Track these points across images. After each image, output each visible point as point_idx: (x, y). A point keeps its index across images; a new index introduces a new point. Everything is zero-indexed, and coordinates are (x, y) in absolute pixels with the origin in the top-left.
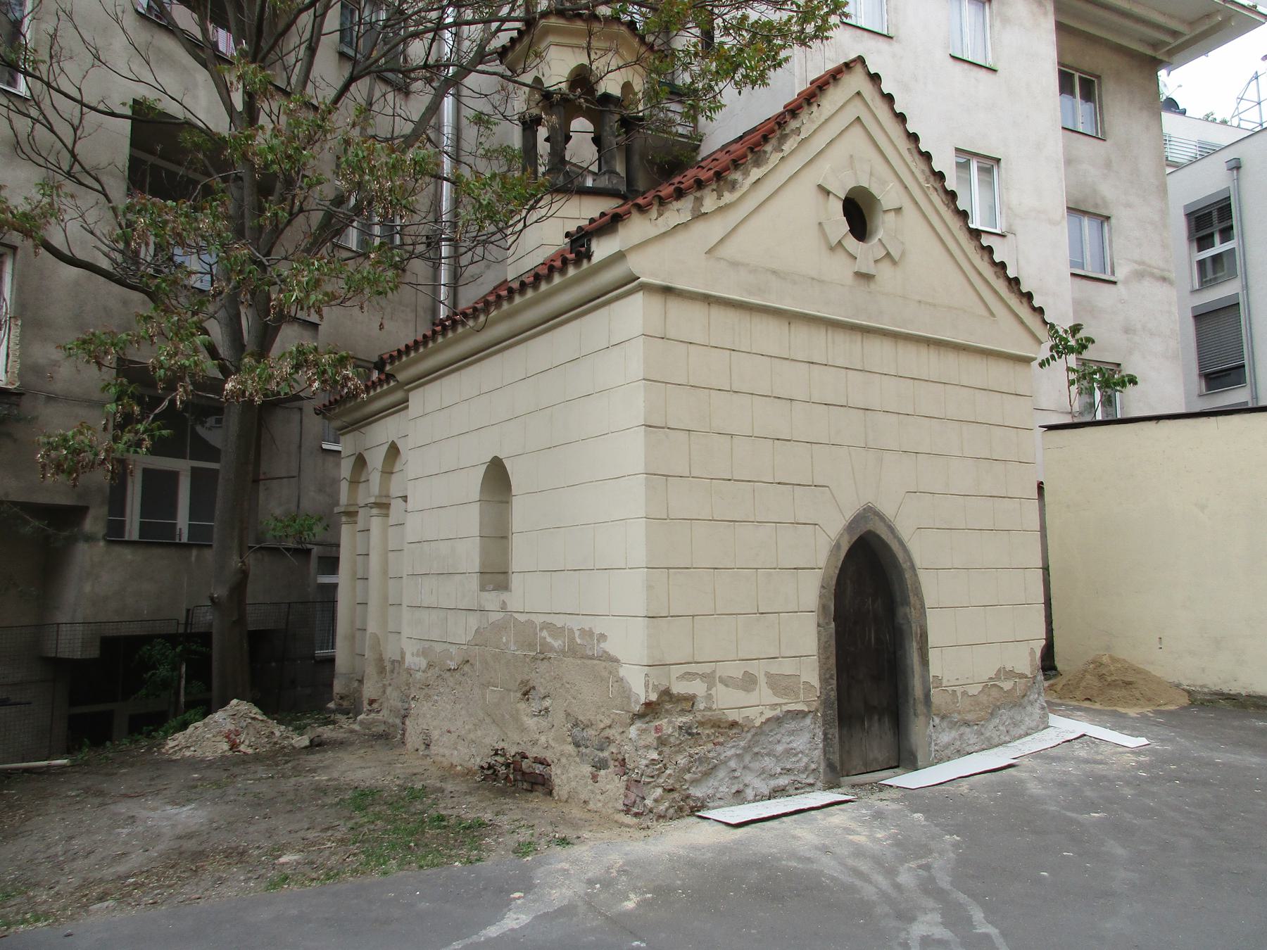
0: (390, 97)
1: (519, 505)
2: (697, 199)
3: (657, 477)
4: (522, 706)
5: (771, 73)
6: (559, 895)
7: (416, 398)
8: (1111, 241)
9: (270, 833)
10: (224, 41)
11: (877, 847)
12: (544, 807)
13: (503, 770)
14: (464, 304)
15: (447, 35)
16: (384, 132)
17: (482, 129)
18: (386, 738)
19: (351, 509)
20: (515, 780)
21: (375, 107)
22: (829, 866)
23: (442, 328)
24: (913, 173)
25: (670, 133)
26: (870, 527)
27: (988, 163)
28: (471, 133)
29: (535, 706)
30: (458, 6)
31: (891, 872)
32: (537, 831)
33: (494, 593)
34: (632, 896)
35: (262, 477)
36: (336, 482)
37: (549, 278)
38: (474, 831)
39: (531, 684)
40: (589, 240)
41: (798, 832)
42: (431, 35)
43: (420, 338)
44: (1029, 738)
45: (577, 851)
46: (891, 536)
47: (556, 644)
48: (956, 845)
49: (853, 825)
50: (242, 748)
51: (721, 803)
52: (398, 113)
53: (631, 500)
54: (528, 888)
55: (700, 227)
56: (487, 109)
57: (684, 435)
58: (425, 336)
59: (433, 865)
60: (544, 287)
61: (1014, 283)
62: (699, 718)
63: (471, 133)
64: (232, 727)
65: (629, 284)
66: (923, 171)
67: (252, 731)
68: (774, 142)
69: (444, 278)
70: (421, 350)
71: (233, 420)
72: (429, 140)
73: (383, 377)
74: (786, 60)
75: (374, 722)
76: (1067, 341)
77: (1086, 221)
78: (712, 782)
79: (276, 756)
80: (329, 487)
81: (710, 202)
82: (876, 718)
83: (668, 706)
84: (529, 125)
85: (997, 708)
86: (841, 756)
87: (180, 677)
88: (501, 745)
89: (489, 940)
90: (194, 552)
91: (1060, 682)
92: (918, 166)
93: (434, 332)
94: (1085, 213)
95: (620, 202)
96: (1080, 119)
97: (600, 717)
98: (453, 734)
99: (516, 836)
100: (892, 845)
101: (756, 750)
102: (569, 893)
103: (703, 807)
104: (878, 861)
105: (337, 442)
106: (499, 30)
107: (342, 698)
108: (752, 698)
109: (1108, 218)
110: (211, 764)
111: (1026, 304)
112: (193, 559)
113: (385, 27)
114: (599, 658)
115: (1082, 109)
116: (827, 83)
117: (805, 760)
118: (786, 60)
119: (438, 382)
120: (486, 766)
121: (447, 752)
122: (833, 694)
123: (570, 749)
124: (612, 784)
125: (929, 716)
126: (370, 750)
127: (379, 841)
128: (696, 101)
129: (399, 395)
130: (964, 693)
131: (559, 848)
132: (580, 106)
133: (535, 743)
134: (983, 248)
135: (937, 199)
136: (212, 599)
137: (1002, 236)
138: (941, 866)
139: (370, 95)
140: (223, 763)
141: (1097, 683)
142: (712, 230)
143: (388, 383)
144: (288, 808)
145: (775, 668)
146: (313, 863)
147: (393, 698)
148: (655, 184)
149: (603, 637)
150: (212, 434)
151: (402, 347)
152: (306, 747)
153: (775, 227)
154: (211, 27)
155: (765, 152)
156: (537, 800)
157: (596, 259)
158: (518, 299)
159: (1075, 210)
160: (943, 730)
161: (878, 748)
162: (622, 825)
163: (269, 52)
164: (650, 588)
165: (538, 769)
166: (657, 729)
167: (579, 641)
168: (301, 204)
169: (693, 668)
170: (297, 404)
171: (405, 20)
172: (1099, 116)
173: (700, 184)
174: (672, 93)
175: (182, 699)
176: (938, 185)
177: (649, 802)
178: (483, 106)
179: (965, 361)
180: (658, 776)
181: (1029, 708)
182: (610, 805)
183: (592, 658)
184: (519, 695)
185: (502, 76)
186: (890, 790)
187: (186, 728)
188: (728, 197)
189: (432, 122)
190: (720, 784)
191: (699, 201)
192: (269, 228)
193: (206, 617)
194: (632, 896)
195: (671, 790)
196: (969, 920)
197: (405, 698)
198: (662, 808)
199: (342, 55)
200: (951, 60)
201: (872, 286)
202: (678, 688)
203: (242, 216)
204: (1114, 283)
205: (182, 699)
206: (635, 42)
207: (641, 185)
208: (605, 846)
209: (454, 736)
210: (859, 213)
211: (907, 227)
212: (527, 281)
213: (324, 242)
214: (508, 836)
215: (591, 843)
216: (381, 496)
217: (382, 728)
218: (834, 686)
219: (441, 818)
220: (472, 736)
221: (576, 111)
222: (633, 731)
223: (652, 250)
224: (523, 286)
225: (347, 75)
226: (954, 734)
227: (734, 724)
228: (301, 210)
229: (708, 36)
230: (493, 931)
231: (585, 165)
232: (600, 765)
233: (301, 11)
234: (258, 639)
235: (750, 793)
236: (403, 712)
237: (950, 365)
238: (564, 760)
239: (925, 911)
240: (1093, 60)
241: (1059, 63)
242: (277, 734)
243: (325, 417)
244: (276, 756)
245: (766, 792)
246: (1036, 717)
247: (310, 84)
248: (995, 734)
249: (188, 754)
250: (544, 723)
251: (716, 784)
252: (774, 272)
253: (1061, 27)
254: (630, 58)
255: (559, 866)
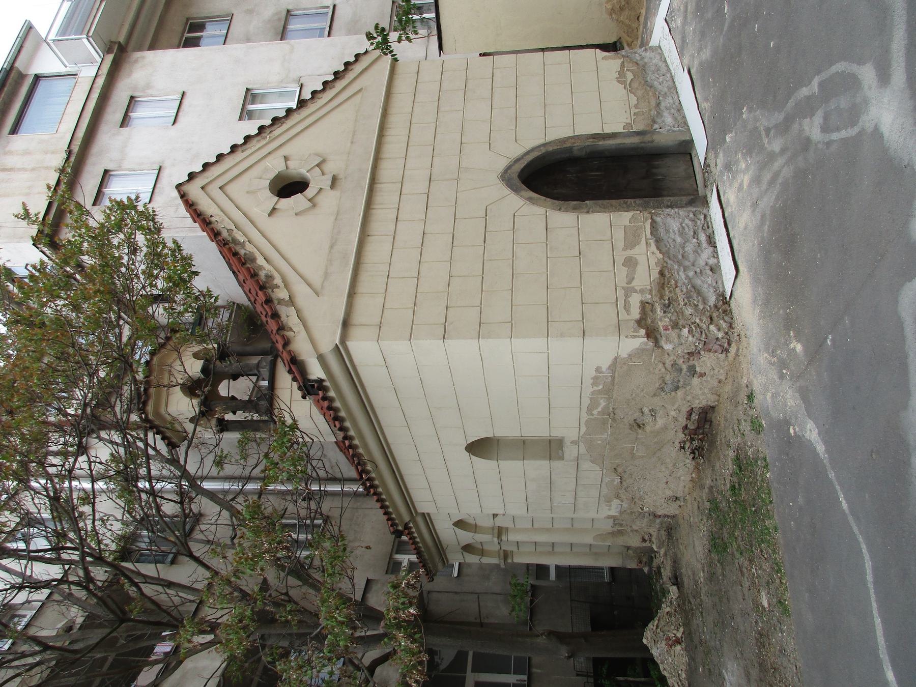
0: (203, 527)
1: (501, 431)
2: (279, 303)
3: (481, 330)
4: (648, 429)
5: (184, 253)
6: (792, 400)
7: (422, 508)
8: (305, 9)
9: (745, 614)
10: (162, 648)
11: (753, 167)
12: (723, 412)
13: (696, 443)
14: (353, 474)
15: (158, 486)
16: (229, 532)
17: (226, 461)
18: (670, 529)
19: (502, 554)
20: (703, 434)
21: (211, 538)
22: (767, 202)
23: (371, 489)
24: (259, 149)
25: (228, 326)
26: (515, 176)
27: (249, 96)
28: (229, 469)
29: (648, 419)
30: (137, 479)
31: (772, 157)
32: (742, 417)
33: (565, 449)
34: (792, 346)
35: (478, 621)
36: (481, 566)
37: (336, 410)
38: (742, 463)
39: (632, 422)
40: (309, 380)
41: (742, 225)
42: (158, 500)
43: (378, 505)
44: (668, 59)
45: (757, 387)
46: (522, 161)
47: (603, 403)
48: (750, 110)
49: (736, 185)
50: (679, 635)
51: (720, 282)
52: (215, 521)
53: (498, 348)
54: (787, 423)
55: (300, 301)
56: (211, 457)
57: (450, 310)
58: (378, 501)
59: (769, 493)
60: (342, 414)
61: (338, 75)
62: (657, 299)
63: (229, 469)
64: (664, 643)
65: (341, 351)
66: (258, 141)
67: (666, 628)
68: (238, 248)
69: (337, 488)
70: (387, 503)
71: (436, 642)
72: (233, 499)
73: (407, 531)
74: (175, 242)
75: (658, 538)
76: (378, 43)
77: (290, 27)
78: (705, 289)
79: (685, 610)
80: (485, 572)
81: (281, 294)
82: (654, 171)
83: (649, 321)
84: (223, 426)
85: (647, 82)
86: (684, 195)
87: (626, 681)
88: (677, 445)
89: (827, 451)
90: (534, 670)
91: (626, 39)
92: (254, 145)
93: (375, 494)
94: (284, 28)
95: (279, 360)
96: (218, 32)
97: (657, 371)
98: (668, 480)
99: (746, 433)
100: (751, 157)
101: (680, 257)
102: (790, 392)
103: (723, 295)
104: (763, 167)
105: (452, 566)
106: (155, 449)
107: (640, 562)
108: (642, 260)
109: (288, 11)
110: (692, 659)
111: (353, 67)
112: (539, 671)
113: (153, 532)
114: (614, 372)
115: (211, 30)
116: (195, 210)
117: (687, 221)
118: (175, 242)
119: (410, 491)
120: (692, 456)
121: (682, 484)
122: (638, 201)
123: (680, 393)
124: (706, 362)
125: (653, 132)
126: (680, 541)
127: (750, 533)
128: (204, 307)
129: (420, 520)
130: (636, 107)
131: (756, 401)
132: (209, 391)
133: (676, 419)
134: (312, 98)
135: (278, 131)
136: (569, 657)
137: (301, 86)
138: (766, 120)
139: (202, 541)
140: (691, 650)
141: (627, 12)
142: (301, 291)
143: (411, 528)
144: (725, 600)
145: (620, 244)
146: (768, 582)
147: (641, 524)
148: (267, 335)
149: (598, 370)
150: (447, 656)
151: (385, 517)
152: (678, 588)
153: (299, 247)
154: (153, 658)
155: (245, 254)
156: (719, 418)
157: (322, 376)
158: (352, 433)
159: (283, 35)
160: (663, 121)
161: (677, 169)
162: (737, 355)
163: (172, 616)
164: (562, 335)
165: (695, 417)
166: (666, 329)
167: (601, 387)
168: (282, 594)
169: (621, 303)
170: (425, 595)
171: (148, 516)
172: (215, 19)
173: (269, 301)
174: (200, 324)
175: (643, 679)
176: (268, 131)
177: (720, 335)
178: (209, 460)
179: (395, 109)
180: (700, 328)
181: (646, 60)
182: (722, 363)
183: (613, 378)
184: (640, 431)
185: (189, 447)
186: (709, 158)
187: (664, 677)
188: (278, 281)
189: (222, 497)
190: (706, 283)
191: (280, 301)
192: (300, 617)
193: (582, 662)
194: (792, 346)
195: (711, 319)
196: (808, 98)
197: (641, 515)
198: (724, 325)
199: (173, 562)
200: (176, 125)
201: (341, 176)
202: (636, 313)
203: (290, 635)
204: (335, 6)
205: (643, 679)
206: (164, 351)
207: (267, 345)
208: (753, 367)
209: (670, 479)
210: (288, 187)
211: (298, 152)
212: (338, 426)
213: (310, 576)
214: (746, 438)
215: (752, 377)
216: (493, 534)
217: (663, 532)
218: (632, 201)
219: (733, 488)
220: (670, 466)
221: (214, 391)
222: (668, 347)
223: (317, 335)
224: (342, 429)
225: (188, 559)
226: (666, 114)
227: (661, 273)
228: (287, 594)
229: (157, 299)
230: (820, 448)
231: (252, 386)
232: (692, 371)
233: (142, 594)
234: (597, 624)
235: (712, 261)
236: (651, 517)
237: (397, 121)
238: (689, 398)
239: (801, 131)
240: (176, 23)
241: (178, 47)
242: (668, 609)
243: (435, 575)
244: (685, 610)
245: (711, 249)
246: (652, 55)
247: (196, 586)
248: (665, 84)
249: (684, 676)
250: (661, 413)
251: (706, 286)
252: (332, 247)
253: (152, 47)
254: (175, 354)
255: (769, 400)
